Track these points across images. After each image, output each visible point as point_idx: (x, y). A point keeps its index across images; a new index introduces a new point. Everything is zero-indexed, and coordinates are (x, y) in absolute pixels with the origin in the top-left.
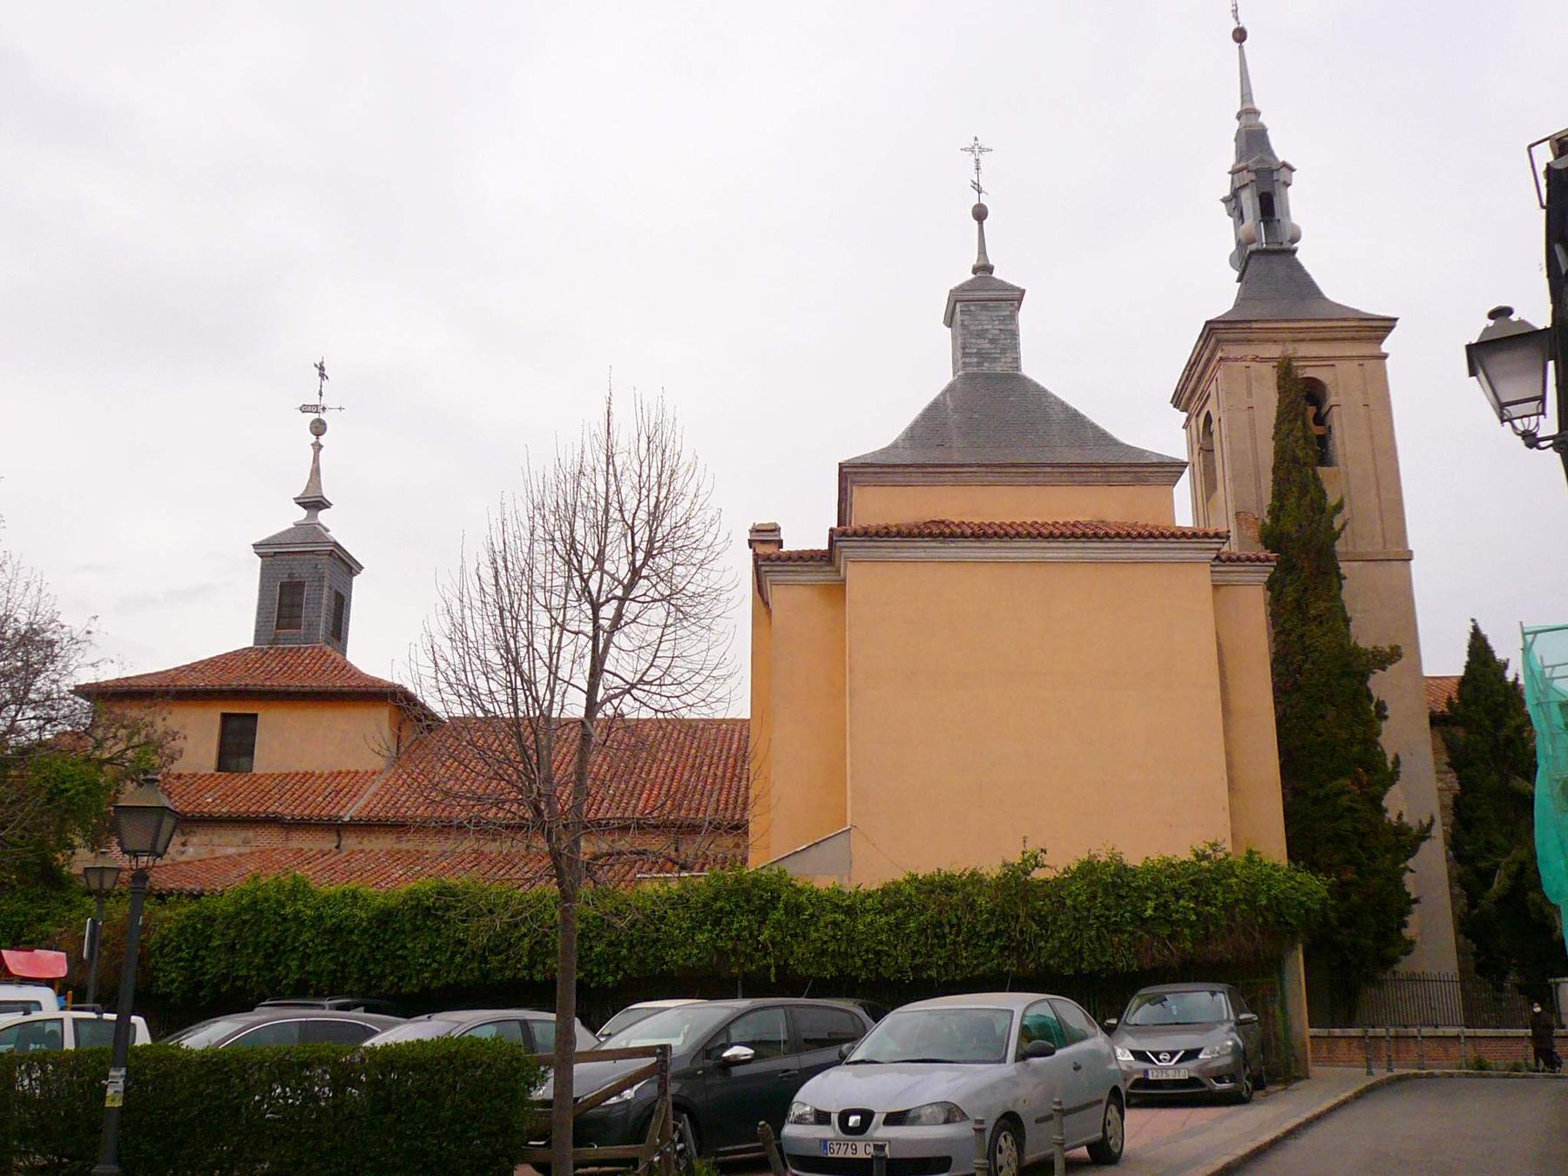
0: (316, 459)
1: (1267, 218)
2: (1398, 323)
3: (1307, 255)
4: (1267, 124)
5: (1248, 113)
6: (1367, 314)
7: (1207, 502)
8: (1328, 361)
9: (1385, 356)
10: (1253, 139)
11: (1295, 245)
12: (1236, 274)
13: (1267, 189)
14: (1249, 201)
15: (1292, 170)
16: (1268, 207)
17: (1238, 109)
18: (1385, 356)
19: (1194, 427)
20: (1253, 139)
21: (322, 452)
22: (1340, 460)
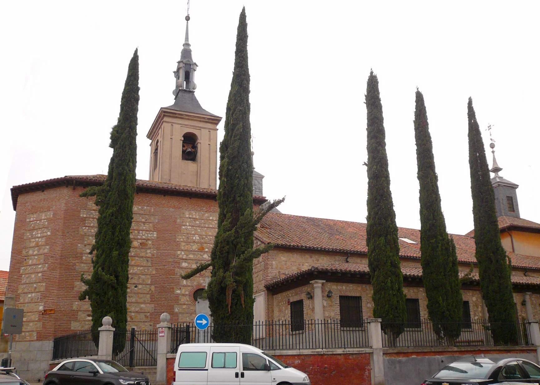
0: (494, 156)
1: (187, 80)
2: (222, 119)
3: (198, 94)
4: (192, 50)
5: (187, 45)
6: (212, 114)
7: (154, 170)
8: (200, 128)
9: (218, 129)
10: (186, 53)
11: (194, 90)
12: (174, 97)
13: (188, 70)
14: (182, 74)
15: (197, 66)
16: (188, 77)
17: (184, 43)
18: (218, 129)
19: (153, 145)
20: (186, 53)
21: (495, 154)
22: (199, 161)
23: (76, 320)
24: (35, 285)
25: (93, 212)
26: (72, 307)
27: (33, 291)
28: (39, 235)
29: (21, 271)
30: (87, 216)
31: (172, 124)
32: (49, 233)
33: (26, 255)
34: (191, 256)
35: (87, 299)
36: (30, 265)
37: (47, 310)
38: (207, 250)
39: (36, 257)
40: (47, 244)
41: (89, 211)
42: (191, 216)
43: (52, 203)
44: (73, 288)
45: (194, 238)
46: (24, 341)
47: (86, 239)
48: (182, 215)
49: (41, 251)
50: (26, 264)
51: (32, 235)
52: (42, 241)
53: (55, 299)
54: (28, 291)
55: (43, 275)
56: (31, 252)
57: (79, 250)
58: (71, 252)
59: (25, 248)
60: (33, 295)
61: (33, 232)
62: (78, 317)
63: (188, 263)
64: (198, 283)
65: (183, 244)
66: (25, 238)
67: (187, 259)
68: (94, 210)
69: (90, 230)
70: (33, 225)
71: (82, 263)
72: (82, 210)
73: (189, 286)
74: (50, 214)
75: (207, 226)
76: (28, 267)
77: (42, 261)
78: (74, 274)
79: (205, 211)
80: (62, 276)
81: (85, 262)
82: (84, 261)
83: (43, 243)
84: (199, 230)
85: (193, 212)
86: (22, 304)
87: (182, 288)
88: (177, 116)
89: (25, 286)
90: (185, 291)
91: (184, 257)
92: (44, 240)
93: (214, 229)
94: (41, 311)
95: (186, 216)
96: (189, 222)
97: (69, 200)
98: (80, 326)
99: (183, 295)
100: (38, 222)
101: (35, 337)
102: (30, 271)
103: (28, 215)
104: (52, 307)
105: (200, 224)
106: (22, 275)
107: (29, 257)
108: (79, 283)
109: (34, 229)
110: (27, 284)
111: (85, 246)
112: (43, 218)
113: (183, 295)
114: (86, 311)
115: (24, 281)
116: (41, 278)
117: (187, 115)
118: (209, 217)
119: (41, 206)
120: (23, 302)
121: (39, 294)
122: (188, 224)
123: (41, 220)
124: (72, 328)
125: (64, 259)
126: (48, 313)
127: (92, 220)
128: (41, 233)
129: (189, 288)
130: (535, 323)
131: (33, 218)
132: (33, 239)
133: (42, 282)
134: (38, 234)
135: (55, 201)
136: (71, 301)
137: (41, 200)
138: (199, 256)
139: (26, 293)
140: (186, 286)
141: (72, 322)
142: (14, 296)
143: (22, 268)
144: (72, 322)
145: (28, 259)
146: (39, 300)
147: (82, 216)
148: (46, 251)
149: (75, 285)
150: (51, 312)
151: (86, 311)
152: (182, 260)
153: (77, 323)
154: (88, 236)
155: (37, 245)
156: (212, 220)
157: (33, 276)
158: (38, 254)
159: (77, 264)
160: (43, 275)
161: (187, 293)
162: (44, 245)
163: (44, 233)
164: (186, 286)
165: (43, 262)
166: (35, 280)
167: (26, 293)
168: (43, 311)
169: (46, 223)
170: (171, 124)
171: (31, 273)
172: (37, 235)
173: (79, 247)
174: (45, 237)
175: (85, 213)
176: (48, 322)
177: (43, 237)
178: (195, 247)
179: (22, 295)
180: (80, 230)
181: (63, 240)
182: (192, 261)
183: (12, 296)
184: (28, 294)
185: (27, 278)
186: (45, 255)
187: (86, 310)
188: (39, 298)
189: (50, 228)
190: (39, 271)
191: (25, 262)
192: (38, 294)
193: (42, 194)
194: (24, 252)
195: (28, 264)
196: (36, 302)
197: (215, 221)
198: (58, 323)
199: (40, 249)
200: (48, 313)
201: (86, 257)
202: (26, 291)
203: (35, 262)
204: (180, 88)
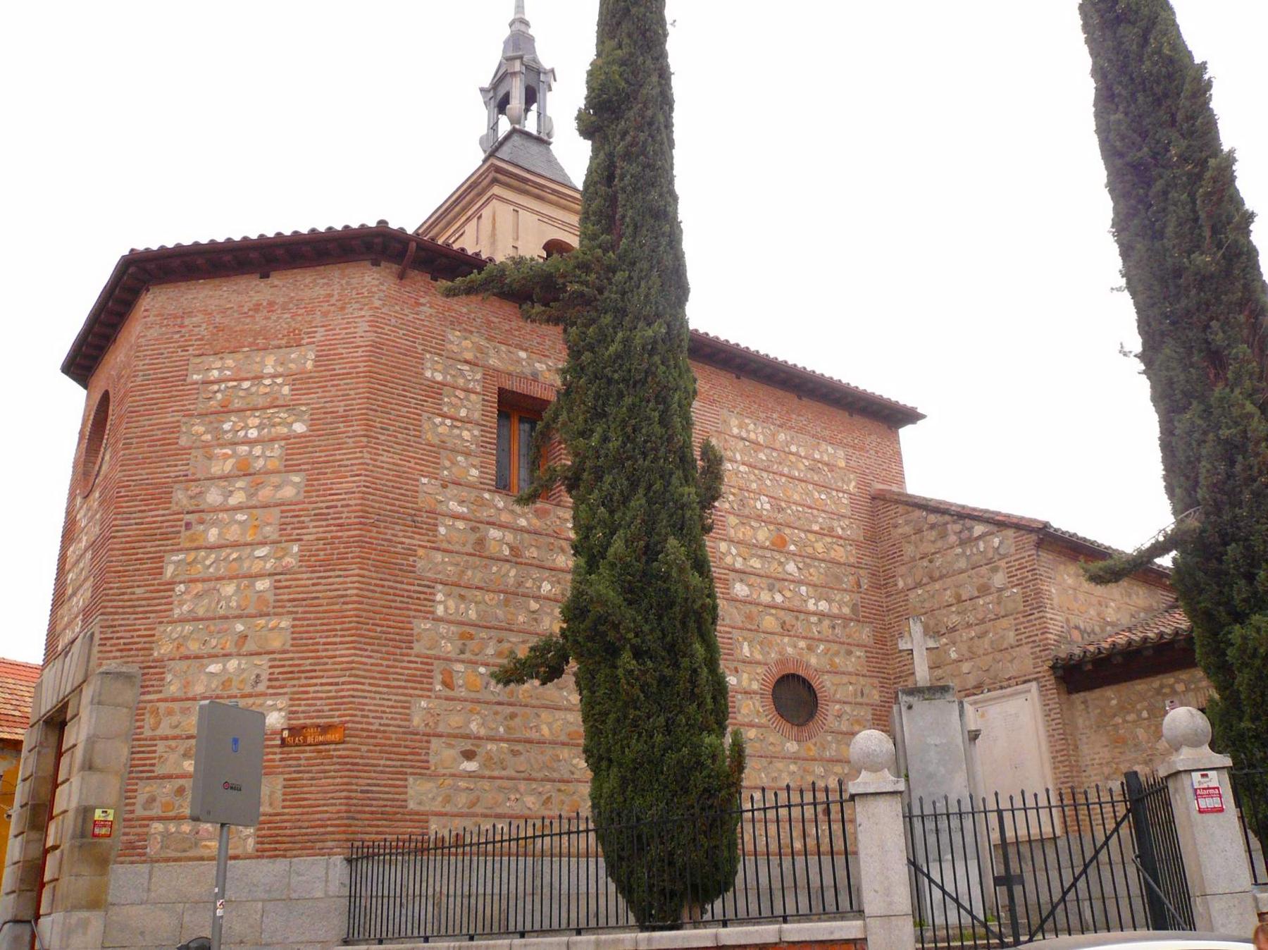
13: (533, 84)
23: (423, 770)
24: (240, 627)
25: (466, 367)
26: (408, 718)
27: (230, 648)
28: (253, 434)
29: (169, 571)
30: (445, 377)
31: (517, 208)
32: (299, 428)
33: (191, 508)
34: (755, 563)
35: (568, 679)
36: (212, 548)
37: (304, 727)
38: (792, 548)
39: (240, 517)
40: (290, 468)
41: (451, 362)
42: (744, 434)
43: (309, 318)
44: (410, 643)
45: (758, 505)
46: (190, 859)
47: (447, 464)
48: (721, 427)
49: (265, 494)
50: (192, 540)
51: (218, 433)
52: (266, 457)
53: (343, 683)
54: (206, 650)
55: (276, 588)
56: (213, 497)
57: (423, 501)
58: (397, 503)
59: (189, 480)
60: (233, 664)
61: (224, 422)
62: (431, 758)
63: (748, 585)
64: (780, 653)
65: (732, 520)
66: (183, 441)
67: (744, 573)
68: (467, 362)
69: (456, 431)
70: (219, 396)
71: (438, 549)
72: (428, 356)
73: (759, 663)
74: (306, 359)
75: (786, 470)
76: (203, 553)
77: (270, 531)
78: (412, 588)
79: (778, 422)
80: (370, 594)
81: (445, 545)
82: (442, 541)
83: (275, 464)
84: (768, 483)
85: (747, 421)
86: (174, 700)
87: (741, 666)
88: (527, 187)
89: (188, 628)
90: (751, 680)
91: (739, 564)
92: (277, 450)
93: (803, 485)
94: (274, 733)
95: (731, 430)
96: (742, 452)
97: (383, 310)
98: (440, 799)
99: (746, 693)
100: (246, 385)
101: (251, 842)
102: (211, 570)
103: (198, 360)
104: (332, 717)
105: (770, 464)
106: (174, 583)
107: (207, 517)
108: (428, 626)
109: (225, 410)
110: (202, 619)
111: (444, 486)
112: (269, 370)
113: (746, 693)
114: (456, 736)
115: (185, 608)
116: (270, 597)
117: (554, 192)
118: (788, 444)
119: (257, 327)
120: (180, 694)
121: (263, 661)
122: (738, 457)
123: (258, 378)
124: (412, 805)
125: (373, 525)
126: (310, 740)
127: (461, 394)
128: (260, 427)
129: (759, 671)
130: (888, 797)
131: (221, 369)
132: (222, 446)
133: (275, 614)
134: (246, 427)
135: (325, 314)
136: (406, 695)
137: (257, 308)
138: (775, 565)
139: (197, 657)
140: (750, 663)
141: (411, 779)
142: (134, 669)
143: (175, 558)
144: (411, 779)
145: (202, 522)
146: (261, 688)
147: (428, 374)
148: (288, 492)
149: (415, 632)
150: (329, 737)
151: (456, 736)
152: (732, 575)
153: (430, 785)
154: (452, 451)
155: (244, 470)
156: (796, 454)
157: (229, 589)
158: (250, 504)
159: (421, 552)
160: (276, 588)
161: (755, 686)
162: (279, 472)
163: (274, 426)
164: (750, 663)
165: (275, 537)
166: (239, 607)
167: (197, 657)
168: (286, 734)
169: (286, 390)
170: (512, 208)
171: (219, 579)
172: (242, 434)
173: (425, 489)
174: (283, 443)
175: (439, 367)
176: (312, 779)
177: (272, 440)
178: (763, 535)
179: (181, 666)
180: (426, 426)
181: (366, 455)
182: (758, 580)
183: (124, 669)
184: (205, 661)
185: (199, 596)
186: (284, 508)
187: (457, 731)
188: (265, 676)
189: (304, 408)
190: (256, 567)
191: (185, 534)
192: (257, 660)
193: (262, 284)
194: (180, 497)
195: (205, 544)
196: (250, 696)
197: (804, 460)
198: (361, 781)
199: (259, 485)
200: (310, 740)
201: (446, 526)
202: (194, 647)
203: (233, 534)
204: (517, 126)
